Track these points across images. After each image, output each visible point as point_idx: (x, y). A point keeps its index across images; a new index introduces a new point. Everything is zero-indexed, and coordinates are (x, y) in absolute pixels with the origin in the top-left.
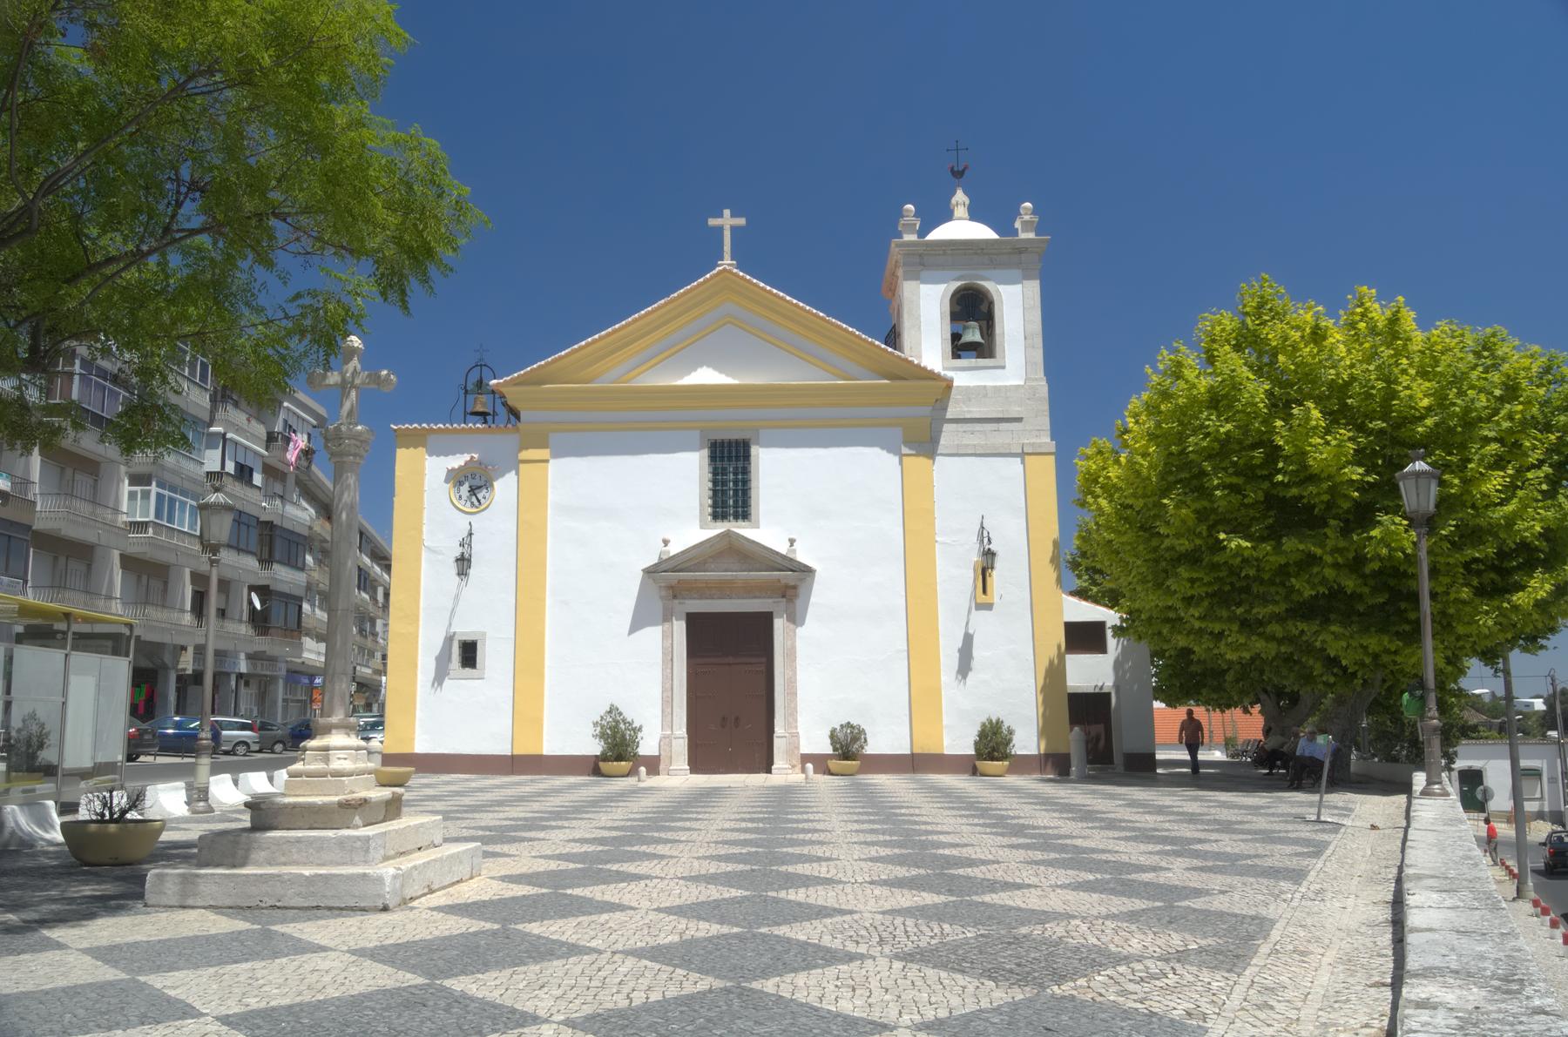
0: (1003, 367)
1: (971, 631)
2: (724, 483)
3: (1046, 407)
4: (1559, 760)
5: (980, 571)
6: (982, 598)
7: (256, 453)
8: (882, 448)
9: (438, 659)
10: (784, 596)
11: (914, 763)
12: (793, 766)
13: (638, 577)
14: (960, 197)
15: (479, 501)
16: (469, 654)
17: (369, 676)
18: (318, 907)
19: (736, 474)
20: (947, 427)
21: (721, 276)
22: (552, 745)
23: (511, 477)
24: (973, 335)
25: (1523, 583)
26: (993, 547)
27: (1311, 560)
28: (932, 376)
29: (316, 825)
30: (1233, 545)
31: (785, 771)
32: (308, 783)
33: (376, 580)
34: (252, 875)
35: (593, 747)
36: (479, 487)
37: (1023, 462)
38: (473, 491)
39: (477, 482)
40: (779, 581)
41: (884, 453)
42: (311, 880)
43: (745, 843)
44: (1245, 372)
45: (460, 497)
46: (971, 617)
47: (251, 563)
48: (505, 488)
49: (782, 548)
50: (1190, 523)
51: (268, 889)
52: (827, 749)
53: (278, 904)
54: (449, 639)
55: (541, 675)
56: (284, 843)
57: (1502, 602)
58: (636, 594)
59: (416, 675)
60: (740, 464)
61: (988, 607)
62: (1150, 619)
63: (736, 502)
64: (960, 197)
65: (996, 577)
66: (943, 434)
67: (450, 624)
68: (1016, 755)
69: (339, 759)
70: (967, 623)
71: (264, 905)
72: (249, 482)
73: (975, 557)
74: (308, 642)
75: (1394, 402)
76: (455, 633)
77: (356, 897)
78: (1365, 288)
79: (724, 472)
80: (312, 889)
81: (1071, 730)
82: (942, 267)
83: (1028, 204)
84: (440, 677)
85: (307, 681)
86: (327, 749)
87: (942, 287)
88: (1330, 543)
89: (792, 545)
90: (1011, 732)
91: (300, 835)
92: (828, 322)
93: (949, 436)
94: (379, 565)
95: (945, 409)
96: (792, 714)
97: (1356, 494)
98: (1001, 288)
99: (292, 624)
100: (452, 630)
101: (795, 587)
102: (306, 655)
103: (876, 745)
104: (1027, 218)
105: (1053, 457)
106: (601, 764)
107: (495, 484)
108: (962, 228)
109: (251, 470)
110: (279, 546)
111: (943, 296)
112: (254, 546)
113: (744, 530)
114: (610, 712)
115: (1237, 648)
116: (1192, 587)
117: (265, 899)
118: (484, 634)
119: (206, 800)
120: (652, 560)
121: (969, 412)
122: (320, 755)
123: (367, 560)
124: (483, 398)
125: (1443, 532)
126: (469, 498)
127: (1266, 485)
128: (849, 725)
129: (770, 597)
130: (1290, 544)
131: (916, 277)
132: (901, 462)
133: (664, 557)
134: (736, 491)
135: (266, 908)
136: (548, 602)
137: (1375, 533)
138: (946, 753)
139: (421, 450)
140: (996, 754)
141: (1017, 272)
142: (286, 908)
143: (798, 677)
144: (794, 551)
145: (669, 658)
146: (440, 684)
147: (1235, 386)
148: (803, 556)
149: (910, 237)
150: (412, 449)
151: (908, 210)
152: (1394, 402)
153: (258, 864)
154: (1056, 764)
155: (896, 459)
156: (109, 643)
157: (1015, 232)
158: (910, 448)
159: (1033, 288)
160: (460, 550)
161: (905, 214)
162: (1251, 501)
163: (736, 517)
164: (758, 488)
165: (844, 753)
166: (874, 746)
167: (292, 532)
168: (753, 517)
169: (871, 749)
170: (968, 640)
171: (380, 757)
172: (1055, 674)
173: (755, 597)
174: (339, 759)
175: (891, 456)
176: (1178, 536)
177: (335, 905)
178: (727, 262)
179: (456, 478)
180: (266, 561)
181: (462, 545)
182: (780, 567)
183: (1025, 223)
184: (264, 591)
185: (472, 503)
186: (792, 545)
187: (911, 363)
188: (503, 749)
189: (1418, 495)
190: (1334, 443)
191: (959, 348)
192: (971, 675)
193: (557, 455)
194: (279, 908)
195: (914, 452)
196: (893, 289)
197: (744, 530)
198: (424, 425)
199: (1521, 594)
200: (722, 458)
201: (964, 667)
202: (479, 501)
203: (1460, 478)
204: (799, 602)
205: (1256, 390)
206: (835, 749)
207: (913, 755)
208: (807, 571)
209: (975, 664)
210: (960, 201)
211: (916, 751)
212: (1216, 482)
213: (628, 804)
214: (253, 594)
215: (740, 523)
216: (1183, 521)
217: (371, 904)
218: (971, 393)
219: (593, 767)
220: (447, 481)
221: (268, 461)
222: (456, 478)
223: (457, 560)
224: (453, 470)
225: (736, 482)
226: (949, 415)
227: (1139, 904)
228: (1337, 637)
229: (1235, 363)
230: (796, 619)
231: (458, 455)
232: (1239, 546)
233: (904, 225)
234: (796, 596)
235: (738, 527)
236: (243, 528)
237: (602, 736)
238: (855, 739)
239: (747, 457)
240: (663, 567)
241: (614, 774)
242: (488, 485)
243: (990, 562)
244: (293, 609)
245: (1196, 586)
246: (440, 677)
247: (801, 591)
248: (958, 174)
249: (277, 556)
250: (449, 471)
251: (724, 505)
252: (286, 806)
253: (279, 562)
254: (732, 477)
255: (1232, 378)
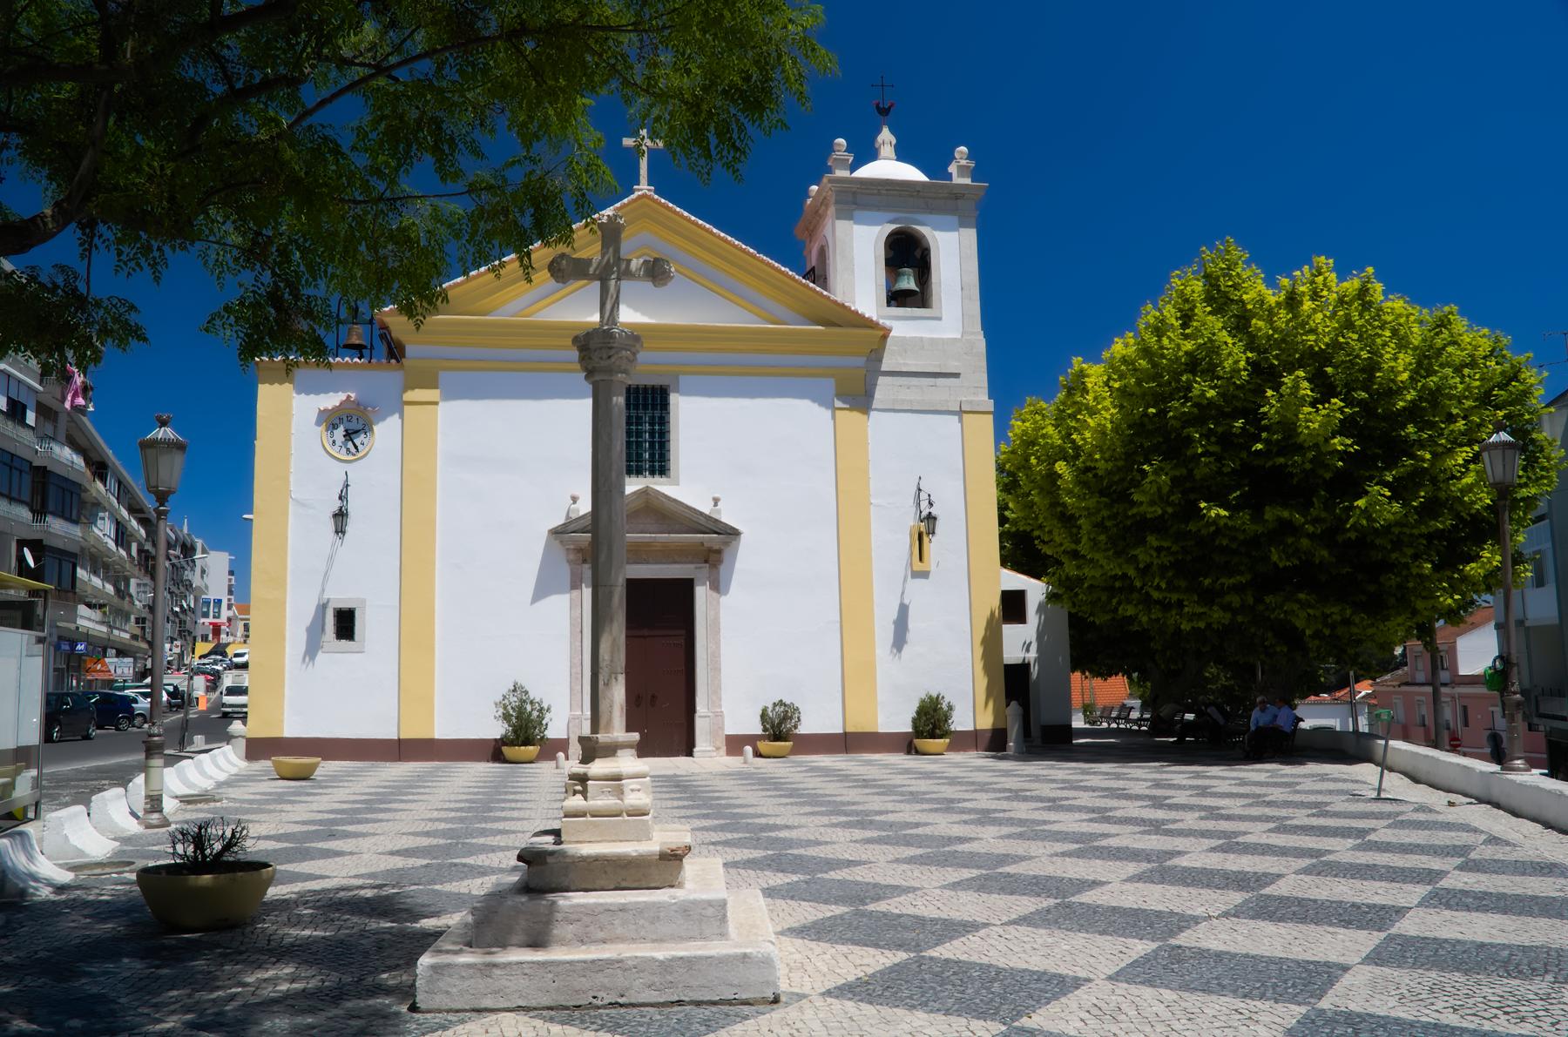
0: (939, 319)
1: (906, 602)
2: (639, 434)
3: (984, 363)
4: (1351, 719)
5: (917, 536)
6: (918, 566)
7: (30, 387)
8: (814, 401)
9: (310, 630)
10: (706, 562)
11: (848, 742)
12: (718, 749)
13: (546, 534)
14: (886, 137)
15: (356, 447)
16: (345, 624)
17: (127, 642)
18: (679, 1003)
19: (652, 424)
20: (882, 380)
21: (639, 202)
22: (444, 729)
23: (394, 420)
24: (908, 283)
25: (1473, 553)
26: (934, 511)
27: (1286, 527)
28: (868, 324)
29: (624, 884)
30: (1213, 513)
31: (709, 754)
32: (595, 825)
33: (132, 535)
34: (578, 962)
35: (495, 729)
36: (357, 432)
37: (961, 421)
38: (349, 435)
39: (353, 426)
40: (702, 544)
41: (815, 406)
42: (667, 966)
43: (457, 810)
44: (1224, 336)
45: (334, 442)
46: (907, 586)
47: (24, 513)
48: (386, 432)
49: (706, 508)
50: (1165, 490)
51: (606, 980)
52: (756, 728)
53: (621, 1001)
54: (323, 607)
55: (431, 649)
56: (600, 913)
57: (1454, 573)
58: (540, 557)
59: (284, 647)
60: (657, 413)
61: (924, 575)
62: (1091, 586)
63: (652, 455)
64: (886, 137)
65: (933, 546)
66: (878, 388)
67: (323, 590)
68: (956, 732)
69: (632, 790)
70: (903, 593)
71: (599, 1003)
72: (21, 420)
73: (910, 521)
74: (82, 610)
75: (1378, 374)
76: (328, 600)
77: (735, 986)
78: (1323, 258)
79: (639, 422)
80: (669, 978)
81: (1008, 705)
82: (877, 207)
83: (963, 149)
84: (312, 649)
85: (67, 648)
86: (617, 778)
87: (876, 230)
88: (1314, 512)
89: (716, 505)
90: (950, 708)
91: (592, 901)
92: (758, 259)
93: (885, 389)
94: (135, 518)
95: (880, 361)
96: (716, 690)
97: (1340, 463)
98: (938, 234)
99: (66, 584)
100: (326, 596)
101: (719, 552)
102: (80, 622)
103: (809, 725)
104: (964, 162)
105: (991, 417)
106: (505, 749)
107: (375, 428)
108: (888, 167)
109: (24, 408)
110: (52, 492)
111: (876, 242)
112: (26, 496)
113: (661, 485)
114: (515, 690)
115: (1193, 617)
116: (1158, 557)
117: (600, 994)
118: (363, 601)
119: (161, 811)
120: (559, 521)
121: (905, 364)
122: (607, 786)
123: (125, 513)
124: (358, 329)
125: (1415, 504)
126: (345, 444)
127: (1244, 455)
128: (781, 703)
129: (692, 563)
130: (1270, 513)
131: (848, 216)
132: (834, 417)
133: (574, 516)
134: (652, 444)
135: (604, 1007)
136: (438, 565)
137: (1361, 503)
138: (880, 731)
139: (288, 386)
140: (938, 731)
141: (954, 219)
142: (633, 1005)
143: (722, 652)
144: (719, 512)
145: (579, 630)
146: (313, 658)
147: (1212, 349)
148: (727, 518)
149: (841, 173)
150: (276, 385)
151: (839, 145)
152: (1378, 374)
153: (563, 942)
154: (995, 742)
155: (829, 413)
156: (18, 614)
157: (950, 177)
158: (844, 402)
159: (970, 236)
160: (338, 504)
161: (836, 148)
162: (1229, 470)
163: (652, 473)
164: (678, 440)
165: (775, 735)
166: (809, 725)
167: (66, 480)
168: (672, 472)
169: (803, 729)
170: (903, 610)
171: (243, 742)
172: (992, 643)
173: (675, 562)
174: (632, 790)
175: (823, 410)
176: (1152, 503)
177: (705, 999)
178: (644, 188)
179: (330, 420)
180: (40, 511)
181: (340, 498)
182: (704, 529)
183: (961, 169)
184: (37, 546)
185: (348, 450)
186: (716, 505)
187: (848, 309)
188: (390, 733)
189: (1504, 466)
190: (1324, 412)
191: (897, 298)
192: (906, 648)
193: (449, 396)
194: (621, 1006)
195: (845, 406)
196: (813, 228)
197: (661, 485)
198: (347, 359)
199: (1473, 565)
200: (637, 407)
201: (900, 640)
202: (356, 447)
203: (1431, 453)
204: (722, 568)
205: (1235, 356)
206: (765, 729)
207: (845, 734)
208: (734, 533)
209: (910, 636)
210: (887, 141)
211: (850, 729)
212: (1200, 450)
213: (377, 774)
214: (26, 550)
215: (657, 478)
216: (1159, 489)
217: (758, 995)
218: (908, 344)
219: (495, 751)
220: (318, 423)
221: (43, 399)
222: (330, 420)
223: (335, 516)
224: (326, 410)
225: (652, 434)
226: (884, 368)
227: (966, 874)
228: (1304, 605)
229: (1214, 326)
230: (717, 587)
231: (331, 394)
232: (1218, 515)
233: (835, 159)
234: (720, 561)
235: (655, 484)
236: (15, 473)
237: (506, 717)
238: (785, 718)
239: (665, 405)
240: (572, 527)
241: (513, 759)
242: (366, 428)
243: (931, 527)
244: (67, 567)
245: (1162, 555)
246: (312, 649)
247: (726, 556)
248: (884, 111)
249: (51, 507)
250: (321, 413)
251: (639, 457)
252: (584, 859)
253: (54, 514)
254: (648, 427)
255: (1210, 340)
